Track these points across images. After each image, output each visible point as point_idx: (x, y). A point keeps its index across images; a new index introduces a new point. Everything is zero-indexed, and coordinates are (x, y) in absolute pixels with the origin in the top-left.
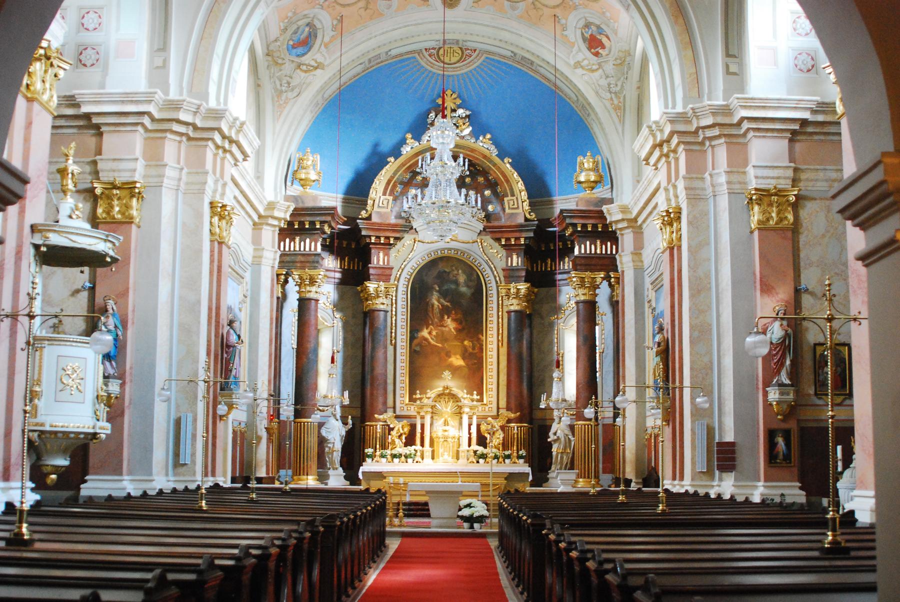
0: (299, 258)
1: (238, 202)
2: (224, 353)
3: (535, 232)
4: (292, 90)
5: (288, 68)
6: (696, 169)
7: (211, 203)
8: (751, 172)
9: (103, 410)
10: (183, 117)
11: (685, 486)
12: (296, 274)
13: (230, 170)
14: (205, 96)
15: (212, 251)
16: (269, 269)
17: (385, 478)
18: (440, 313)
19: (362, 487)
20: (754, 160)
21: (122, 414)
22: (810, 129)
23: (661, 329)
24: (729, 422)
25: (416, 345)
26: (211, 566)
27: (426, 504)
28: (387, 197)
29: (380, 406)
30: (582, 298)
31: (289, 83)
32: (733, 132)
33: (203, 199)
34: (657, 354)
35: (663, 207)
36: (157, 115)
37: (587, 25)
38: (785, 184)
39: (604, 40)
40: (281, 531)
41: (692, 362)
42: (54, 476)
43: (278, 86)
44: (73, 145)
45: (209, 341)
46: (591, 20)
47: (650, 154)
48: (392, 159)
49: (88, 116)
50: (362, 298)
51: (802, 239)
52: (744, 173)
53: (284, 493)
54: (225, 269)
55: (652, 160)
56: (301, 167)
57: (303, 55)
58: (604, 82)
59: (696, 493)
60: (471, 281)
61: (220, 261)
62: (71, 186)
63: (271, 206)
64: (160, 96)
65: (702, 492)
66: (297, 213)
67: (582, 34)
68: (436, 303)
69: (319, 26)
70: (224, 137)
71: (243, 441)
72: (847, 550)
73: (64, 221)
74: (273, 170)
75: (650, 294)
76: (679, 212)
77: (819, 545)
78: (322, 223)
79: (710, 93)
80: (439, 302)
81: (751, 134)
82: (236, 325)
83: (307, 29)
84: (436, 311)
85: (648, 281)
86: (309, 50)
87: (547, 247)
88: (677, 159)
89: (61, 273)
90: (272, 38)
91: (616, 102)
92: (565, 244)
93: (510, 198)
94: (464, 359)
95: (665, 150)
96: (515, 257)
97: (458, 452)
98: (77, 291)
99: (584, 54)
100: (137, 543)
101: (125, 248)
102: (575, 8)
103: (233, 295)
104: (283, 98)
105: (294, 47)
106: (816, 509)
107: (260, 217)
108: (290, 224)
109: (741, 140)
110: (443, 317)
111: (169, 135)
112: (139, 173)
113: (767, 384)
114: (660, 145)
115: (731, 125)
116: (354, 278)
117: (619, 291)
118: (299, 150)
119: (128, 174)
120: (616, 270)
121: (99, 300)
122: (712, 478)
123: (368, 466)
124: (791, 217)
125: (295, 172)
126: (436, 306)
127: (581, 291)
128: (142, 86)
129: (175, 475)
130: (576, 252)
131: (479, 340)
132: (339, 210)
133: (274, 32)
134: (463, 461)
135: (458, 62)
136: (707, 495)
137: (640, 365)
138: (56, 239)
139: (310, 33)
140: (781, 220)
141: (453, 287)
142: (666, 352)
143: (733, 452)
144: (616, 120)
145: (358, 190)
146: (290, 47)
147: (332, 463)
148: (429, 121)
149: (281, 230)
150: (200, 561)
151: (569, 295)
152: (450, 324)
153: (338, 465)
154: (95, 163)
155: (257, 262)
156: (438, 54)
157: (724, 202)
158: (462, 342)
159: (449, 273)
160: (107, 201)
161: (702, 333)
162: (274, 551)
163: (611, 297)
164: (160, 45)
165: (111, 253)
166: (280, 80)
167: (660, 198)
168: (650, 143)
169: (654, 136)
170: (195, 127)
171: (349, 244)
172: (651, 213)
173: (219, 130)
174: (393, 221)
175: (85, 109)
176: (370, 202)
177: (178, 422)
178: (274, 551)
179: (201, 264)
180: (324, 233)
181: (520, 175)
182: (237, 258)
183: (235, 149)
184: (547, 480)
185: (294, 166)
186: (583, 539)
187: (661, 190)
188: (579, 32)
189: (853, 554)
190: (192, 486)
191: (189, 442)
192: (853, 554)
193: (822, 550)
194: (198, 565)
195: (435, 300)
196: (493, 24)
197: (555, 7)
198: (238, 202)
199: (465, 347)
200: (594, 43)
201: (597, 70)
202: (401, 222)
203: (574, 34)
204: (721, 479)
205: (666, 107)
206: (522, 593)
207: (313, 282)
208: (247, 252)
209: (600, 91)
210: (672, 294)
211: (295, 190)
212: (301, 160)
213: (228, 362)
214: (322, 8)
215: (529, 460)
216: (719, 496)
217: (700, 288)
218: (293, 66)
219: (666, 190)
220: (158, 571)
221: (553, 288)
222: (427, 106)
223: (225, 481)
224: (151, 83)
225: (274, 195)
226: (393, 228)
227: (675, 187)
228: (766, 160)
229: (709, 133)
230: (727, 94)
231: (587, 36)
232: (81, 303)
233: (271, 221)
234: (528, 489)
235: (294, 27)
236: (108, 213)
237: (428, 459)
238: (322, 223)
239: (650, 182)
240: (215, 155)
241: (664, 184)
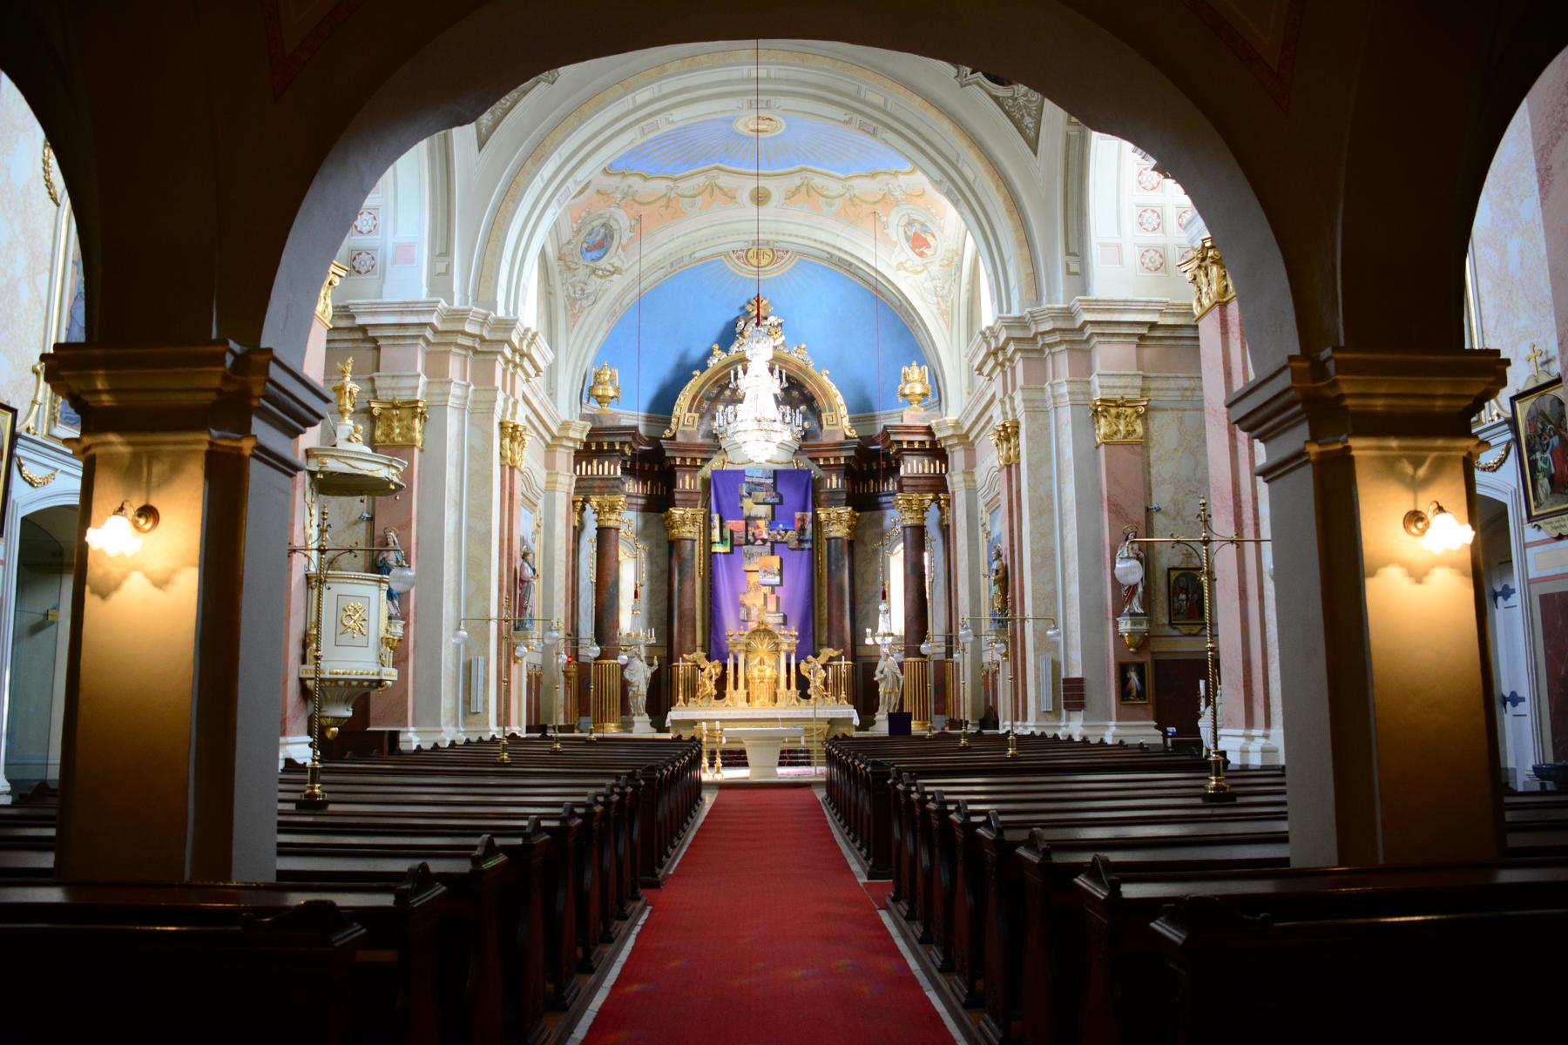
0: (597, 483)
1: (530, 422)
2: (518, 587)
3: (856, 450)
5: (582, 273)
6: (1037, 378)
7: (501, 424)
8: (1096, 381)
9: (389, 655)
10: (469, 328)
11: (1029, 727)
12: (594, 500)
13: (521, 387)
14: (493, 305)
15: (503, 476)
16: (564, 496)
19: (669, 736)
20: (1098, 367)
21: (406, 659)
22: (1158, 333)
23: (999, 555)
24: (1076, 656)
26: (538, 829)
27: (743, 752)
29: (688, 645)
30: (909, 522)
32: (1076, 337)
33: (492, 420)
34: (996, 582)
35: (998, 421)
36: (440, 327)
37: (911, 223)
38: (1132, 394)
39: (930, 238)
40: (602, 786)
41: (1034, 591)
42: (335, 729)
44: (350, 360)
45: (501, 576)
47: (984, 363)
48: (697, 373)
49: (363, 328)
50: (668, 524)
51: (1153, 453)
52: (1089, 382)
53: (589, 742)
54: (518, 496)
55: (986, 370)
56: (597, 382)
59: (1043, 735)
61: (511, 488)
62: (349, 406)
63: (565, 426)
64: (443, 304)
65: (1050, 733)
66: (593, 433)
69: (615, 226)
70: (514, 350)
71: (536, 683)
72: (1233, 796)
73: (342, 445)
74: (567, 387)
75: (985, 517)
76: (1016, 426)
77: (1202, 791)
78: (622, 444)
79: (1049, 294)
81: (1095, 339)
82: (530, 557)
85: (981, 503)
87: (870, 466)
88: (1013, 369)
89: (336, 503)
90: (564, 241)
92: (889, 463)
95: (1001, 359)
98: (355, 523)
99: (906, 254)
100: (425, 799)
101: (407, 475)
102: (897, 203)
103: (525, 524)
105: (588, 250)
106: (1186, 753)
107: (554, 437)
108: (587, 445)
109: (1083, 346)
111: (454, 349)
112: (420, 389)
113: (1118, 613)
114: (995, 353)
115: (1073, 330)
116: (658, 504)
117: (950, 514)
118: (595, 363)
119: (409, 392)
120: (945, 491)
121: (378, 531)
122: (1059, 717)
123: (674, 715)
124: (1140, 429)
125: (591, 389)
127: (908, 515)
128: (423, 295)
129: (465, 725)
130: (902, 472)
132: (642, 430)
133: (567, 234)
136: (1056, 736)
137: (975, 593)
138: (333, 465)
140: (1129, 433)
142: (1005, 580)
143: (1081, 689)
144: (944, 326)
145: (662, 406)
147: (637, 708)
148: (738, 330)
149: (577, 452)
150: (525, 823)
151: (896, 517)
153: (643, 710)
154: (372, 380)
155: (550, 488)
157: (1066, 414)
160: (388, 422)
161: (1045, 558)
162: (598, 809)
163: (941, 521)
164: (442, 249)
165: (396, 480)
167: (996, 411)
168: (984, 351)
169: (989, 344)
170: (483, 340)
171: (651, 468)
172: (983, 428)
173: (510, 343)
174: (700, 440)
175: (360, 321)
176: (674, 420)
177: (468, 667)
178: (598, 809)
179: (491, 491)
180: (624, 454)
181: (838, 388)
182: (528, 483)
183: (526, 363)
184: (874, 723)
185: (590, 382)
186: (932, 786)
187: (997, 402)
188: (901, 230)
189: (1240, 800)
190: (487, 737)
191: (480, 687)
192: (1240, 800)
193: (1205, 796)
194: (524, 828)
198: (530, 422)
202: (709, 441)
203: (896, 232)
204: (1068, 720)
205: (1001, 311)
206: (860, 849)
207: (613, 509)
208: (540, 476)
210: (1011, 516)
211: (593, 407)
212: (597, 375)
213: (522, 598)
214: (619, 206)
215: (854, 701)
216: (1070, 738)
217: (1044, 509)
219: (1002, 402)
220: (486, 836)
221: (876, 514)
222: (736, 313)
223: (518, 729)
224: (432, 292)
225: (567, 413)
226: (701, 448)
227: (1012, 399)
228: (1113, 366)
229: (1049, 339)
230: (1070, 295)
231: (910, 234)
232: (360, 534)
233: (565, 443)
234: (855, 734)
235: (588, 228)
236: (387, 435)
238: (622, 444)
239: (983, 394)
240: (505, 371)
241: (999, 395)
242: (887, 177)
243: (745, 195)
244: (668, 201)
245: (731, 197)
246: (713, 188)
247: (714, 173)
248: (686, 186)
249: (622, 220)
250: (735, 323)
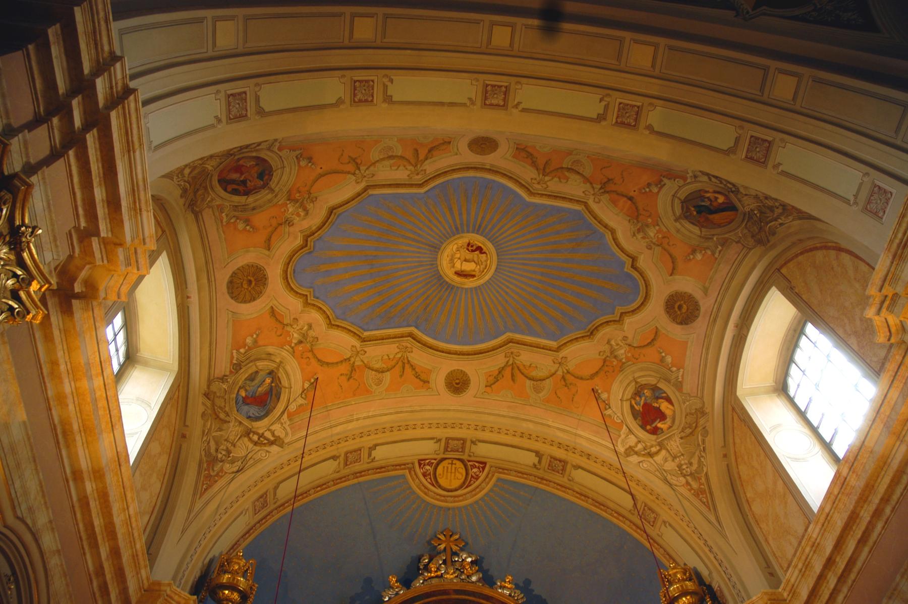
4: (233, 462)
31: (229, 452)
37: (638, 393)
39: (664, 406)
43: (213, 450)
46: (643, 381)
57: (258, 419)
58: (670, 465)
67: (632, 407)
69: (285, 382)
83: (268, 381)
86: (266, 415)
91: (695, 485)
97: (886, 523)
99: (634, 435)
102: (622, 367)
104: (217, 468)
105: (246, 401)
135: (461, 487)
139: (271, 389)
146: (240, 399)
156: (435, 474)
166: (217, 444)
188: (626, 406)
196: (511, 414)
197: (592, 376)
200: (649, 416)
201: (657, 453)
209: (669, 477)
214: (293, 353)
218: (240, 429)
242: (607, 330)
243: (439, 380)
244: (353, 370)
245: (423, 380)
246: (405, 363)
247: (418, 179)
248: (376, 353)
249: (294, 377)
250: (419, 559)
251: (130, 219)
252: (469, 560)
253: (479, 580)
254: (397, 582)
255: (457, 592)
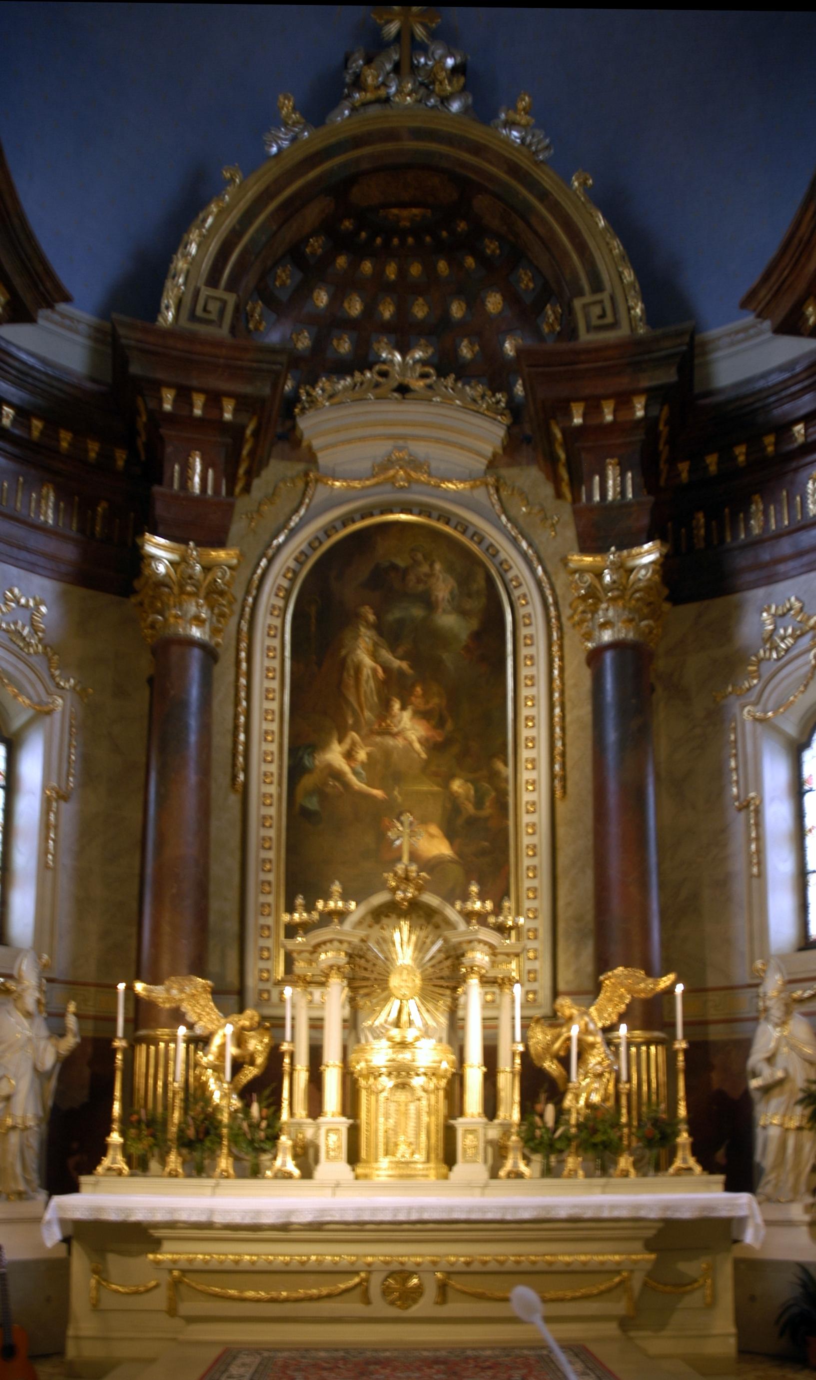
17: (156, 1244)
18: (379, 693)
25: (309, 794)
28: (220, 293)
60: (470, 596)
68: (368, 662)
80: (374, 656)
84: (369, 686)
93: (588, 298)
94: (450, 835)
96: (611, 473)
97: (449, 1134)
110: (386, 705)
126: (366, 672)
131: (495, 777)
134: (471, 1168)
141: (417, 612)
152: (410, 728)
158: (446, 785)
159: (405, 572)
195: (366, 655)
199: (453, 798)
237: (332, 1167)
251: (377, 1131)
252: (450, 62)
253: (465, 110)
254: (294, 109)
255: (418, 134)
